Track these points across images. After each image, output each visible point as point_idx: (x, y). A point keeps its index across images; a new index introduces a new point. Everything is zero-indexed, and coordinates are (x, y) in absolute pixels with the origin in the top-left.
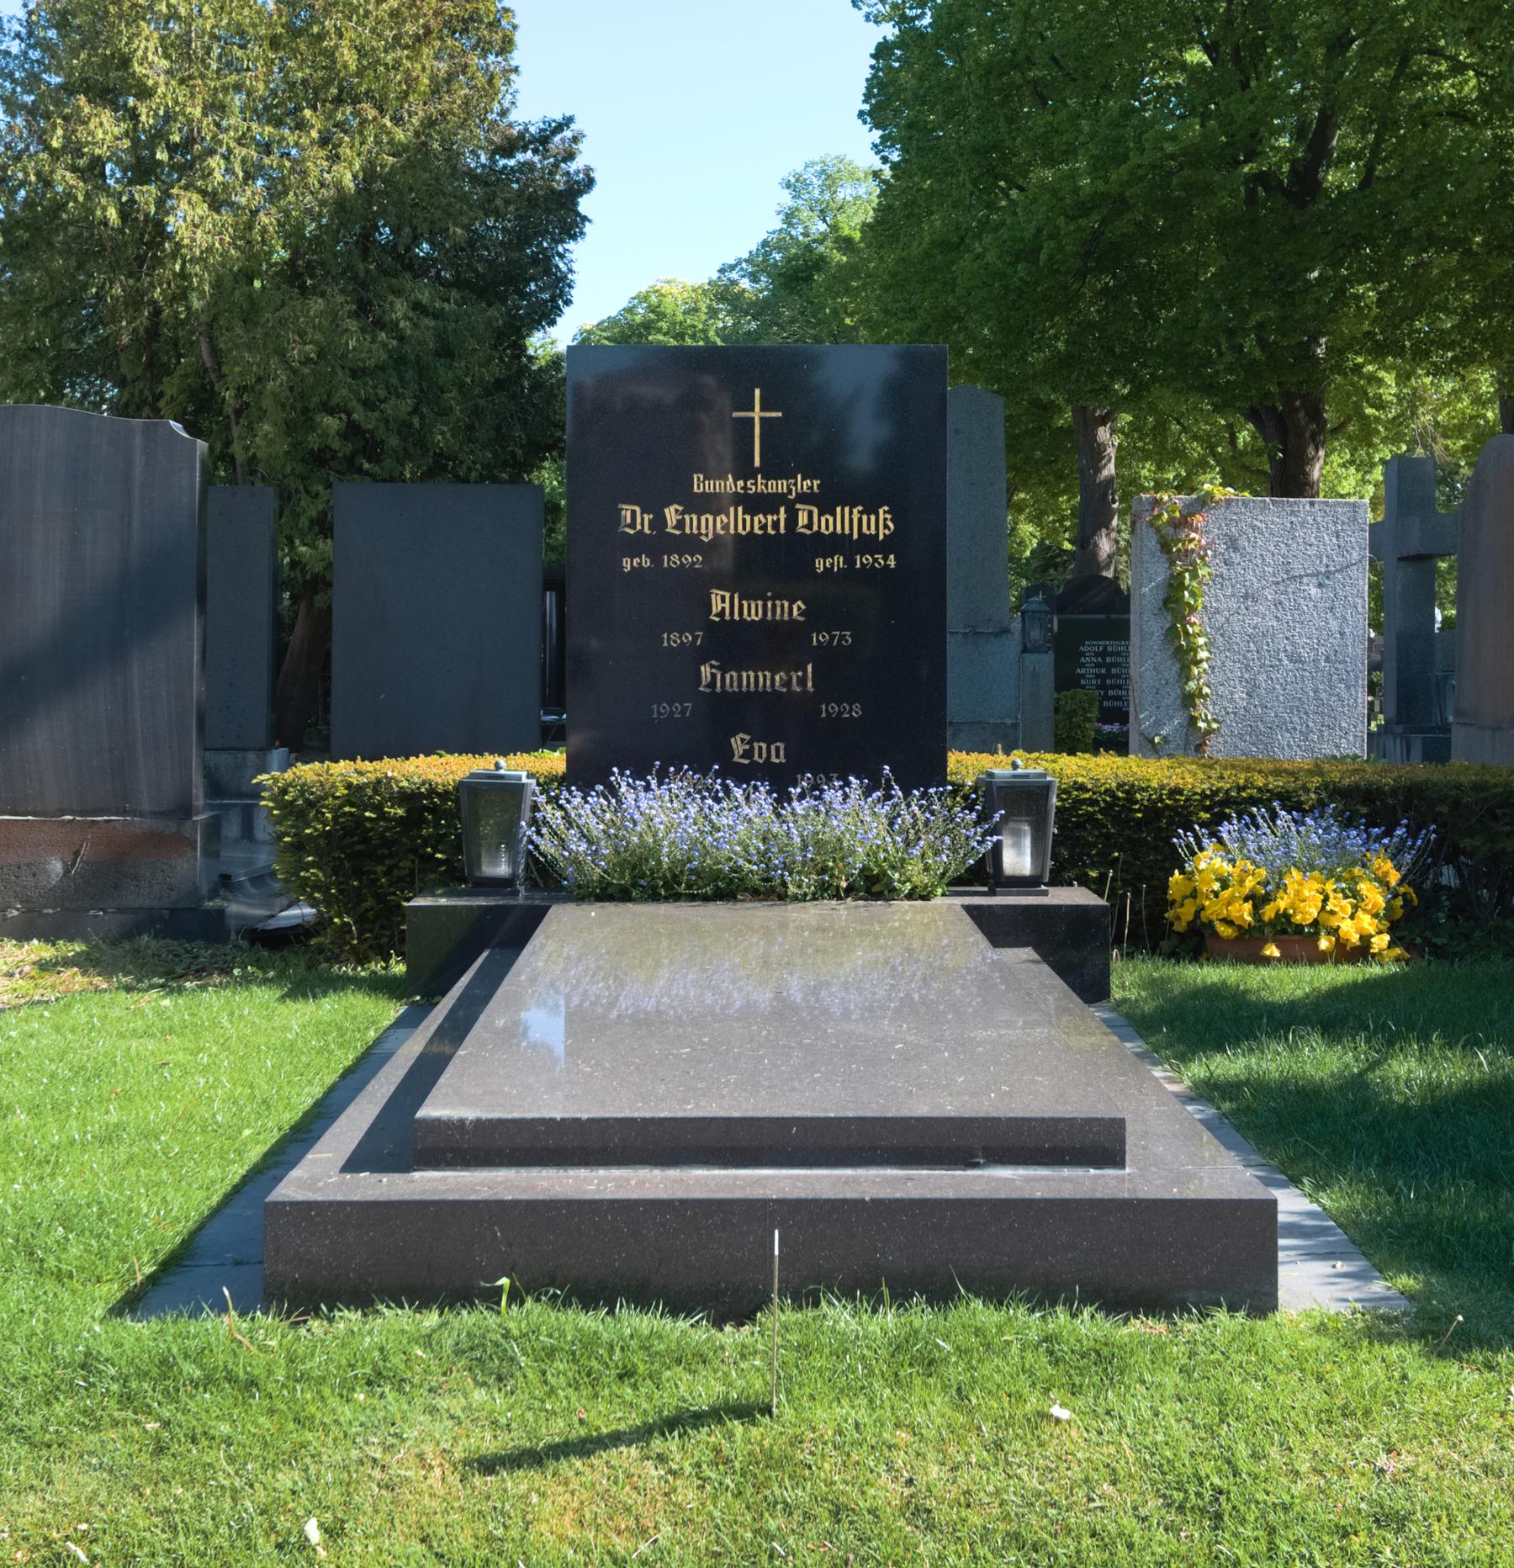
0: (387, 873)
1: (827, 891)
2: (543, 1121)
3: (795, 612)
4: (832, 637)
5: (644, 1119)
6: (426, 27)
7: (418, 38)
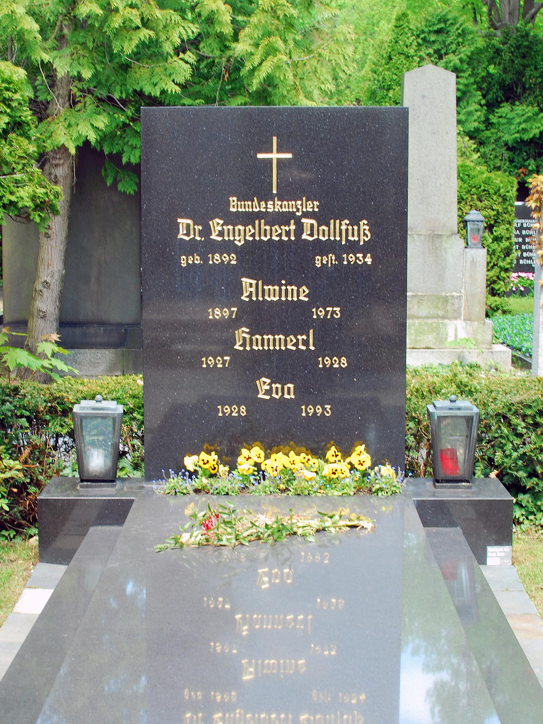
4: (327, 312)
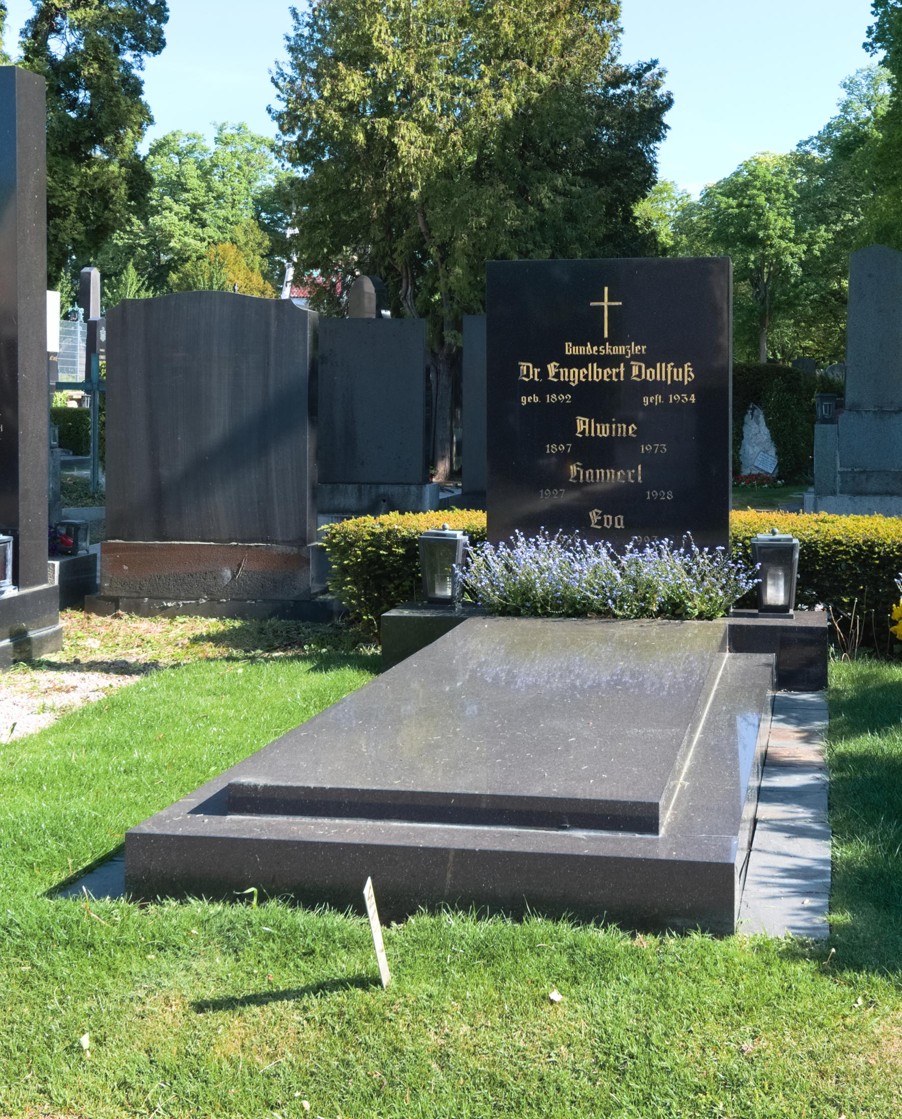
0: (396, 588)
1: (643, 612)
2: (303, 788)
3: (630, 431)
4: (654, 448)
5: (363, 790)
6: (558, 7)
7: (552, 15)
